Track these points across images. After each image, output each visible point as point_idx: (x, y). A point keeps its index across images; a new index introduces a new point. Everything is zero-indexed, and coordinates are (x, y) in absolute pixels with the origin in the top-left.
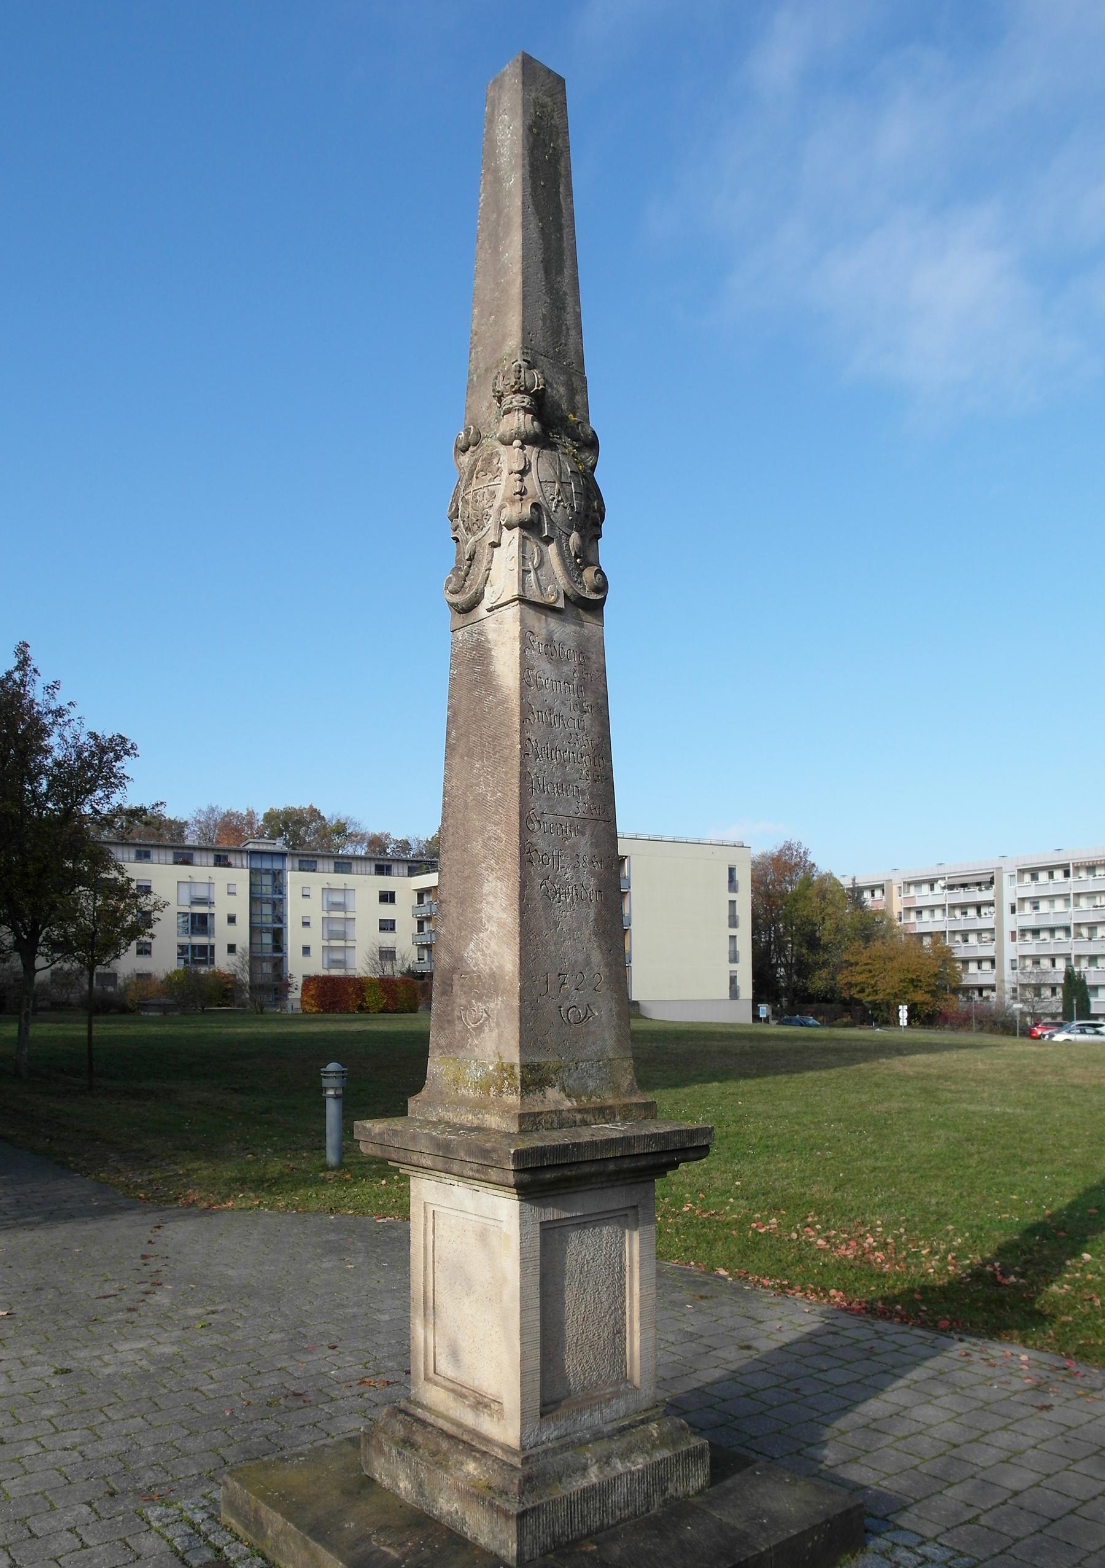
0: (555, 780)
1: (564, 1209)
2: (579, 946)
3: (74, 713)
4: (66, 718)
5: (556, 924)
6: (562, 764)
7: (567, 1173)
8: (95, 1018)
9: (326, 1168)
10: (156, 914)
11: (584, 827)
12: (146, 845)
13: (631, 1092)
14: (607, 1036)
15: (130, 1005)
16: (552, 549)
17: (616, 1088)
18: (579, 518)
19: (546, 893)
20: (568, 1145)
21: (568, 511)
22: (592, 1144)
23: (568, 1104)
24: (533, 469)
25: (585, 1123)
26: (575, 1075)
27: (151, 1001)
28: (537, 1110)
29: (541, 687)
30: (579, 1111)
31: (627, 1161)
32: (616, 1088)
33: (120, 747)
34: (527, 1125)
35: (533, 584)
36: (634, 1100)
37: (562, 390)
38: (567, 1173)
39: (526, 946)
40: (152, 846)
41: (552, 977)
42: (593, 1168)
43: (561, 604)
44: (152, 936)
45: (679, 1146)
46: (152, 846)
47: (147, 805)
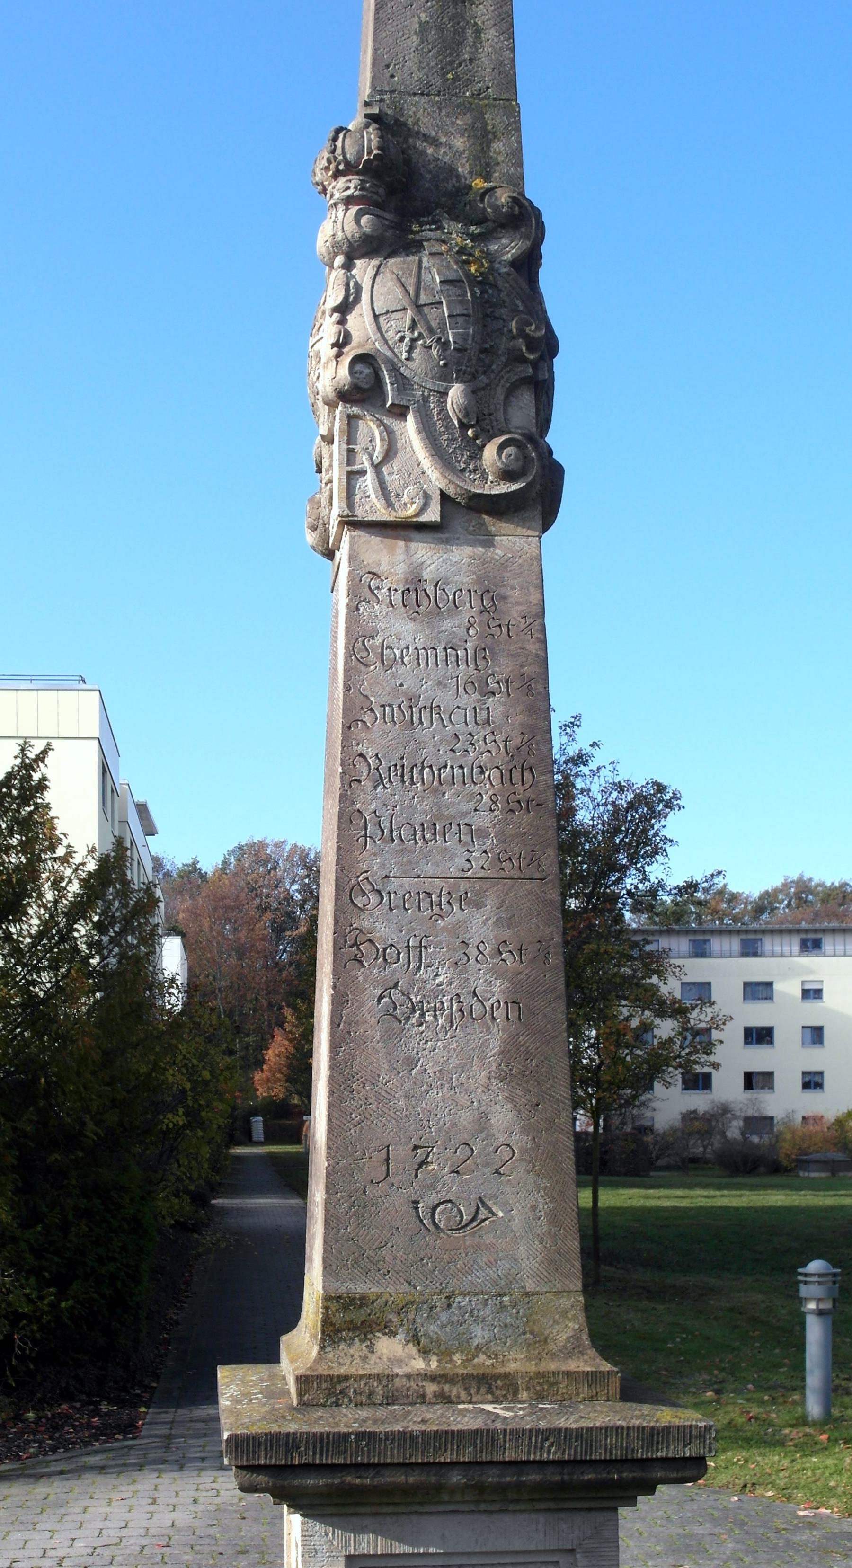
0: (418, 818)
1: (401, 1540)
2: (463, 1099)
3: (599, 758)
4: (593, 766)
5: (411, 1063)
6: (437, 791)
7: (351, 1479)
8: (601, 1178)
9: (803, 1421)
10: (715, 1035)
11: (482, 893)
12: (816, 931)
13: (573, 1350)
14: (522, 1251)
15: (785, 1163)
16: (409, 428)
17: (539, 1342)
18: (502, 354)
19: (390, 1013)
20: (347, 1435)
21: (435, 353)
22: (404, 1438)
23: (419, 1364)
24: (365, 297)
25: (445, 1399)
26: (444, 1317)
27: (813, 1157)
28: (342, 1371)
29: (388, 664)
30: (433, 1378)
31: (495, 1471)
32: (539, 1342)
33: (654, 802)
34: (315, 1394)
35: (371, 492)
36: (572, 1365)
37: (459, 143)
38: (351, 1479)
39: (342, 1099)
40: (824, 931)
41: (400, 1153)
42: (400, 1478)
43: (433, 515)
44: (716, 1066)
45: (617, 1454)
46: (824, 931)
47: (698, 878)
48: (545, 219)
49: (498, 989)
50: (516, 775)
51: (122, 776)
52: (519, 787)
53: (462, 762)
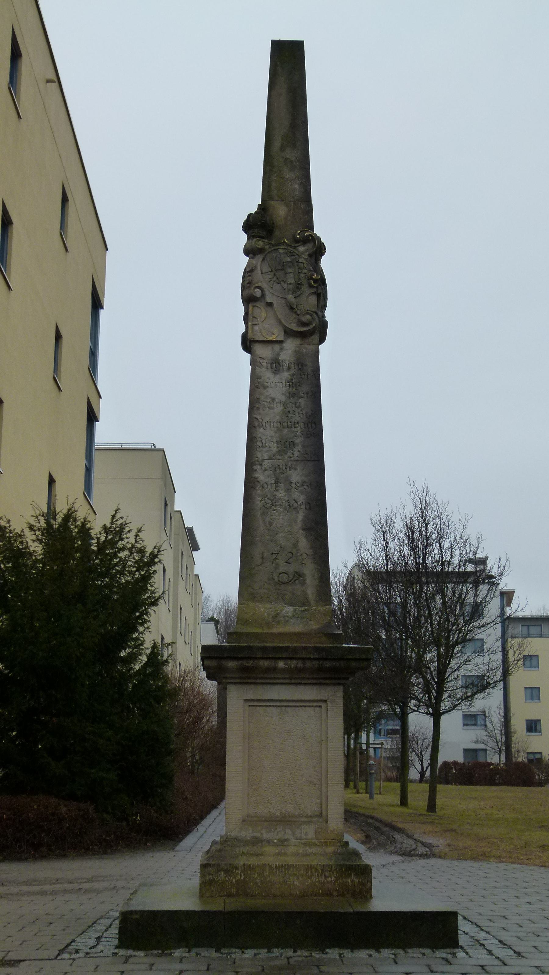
48: (335, 312)
49: (301, 499)
50: (310, 425)
51: (22, 963)
52: (310, 429)
53: (290, 420)
